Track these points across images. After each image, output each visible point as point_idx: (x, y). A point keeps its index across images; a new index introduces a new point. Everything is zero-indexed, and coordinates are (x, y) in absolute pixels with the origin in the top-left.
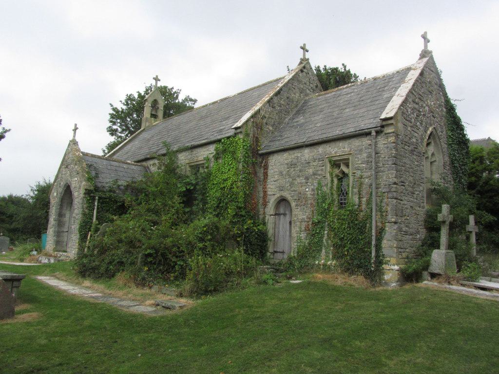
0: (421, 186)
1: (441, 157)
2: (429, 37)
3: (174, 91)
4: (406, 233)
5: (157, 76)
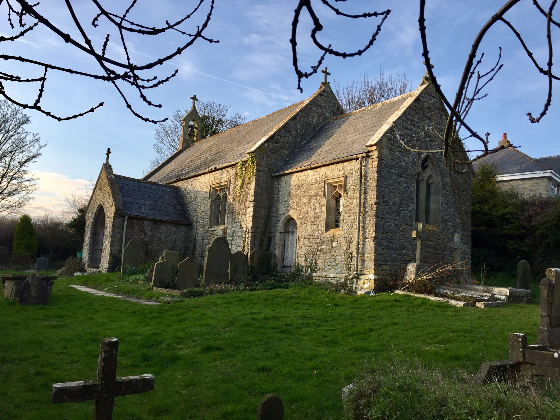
0: (409, 206)
1: (440, 179)
2: (299, 91)
3: (221, 107)
4: (388, 248)
5: (195, 96)
